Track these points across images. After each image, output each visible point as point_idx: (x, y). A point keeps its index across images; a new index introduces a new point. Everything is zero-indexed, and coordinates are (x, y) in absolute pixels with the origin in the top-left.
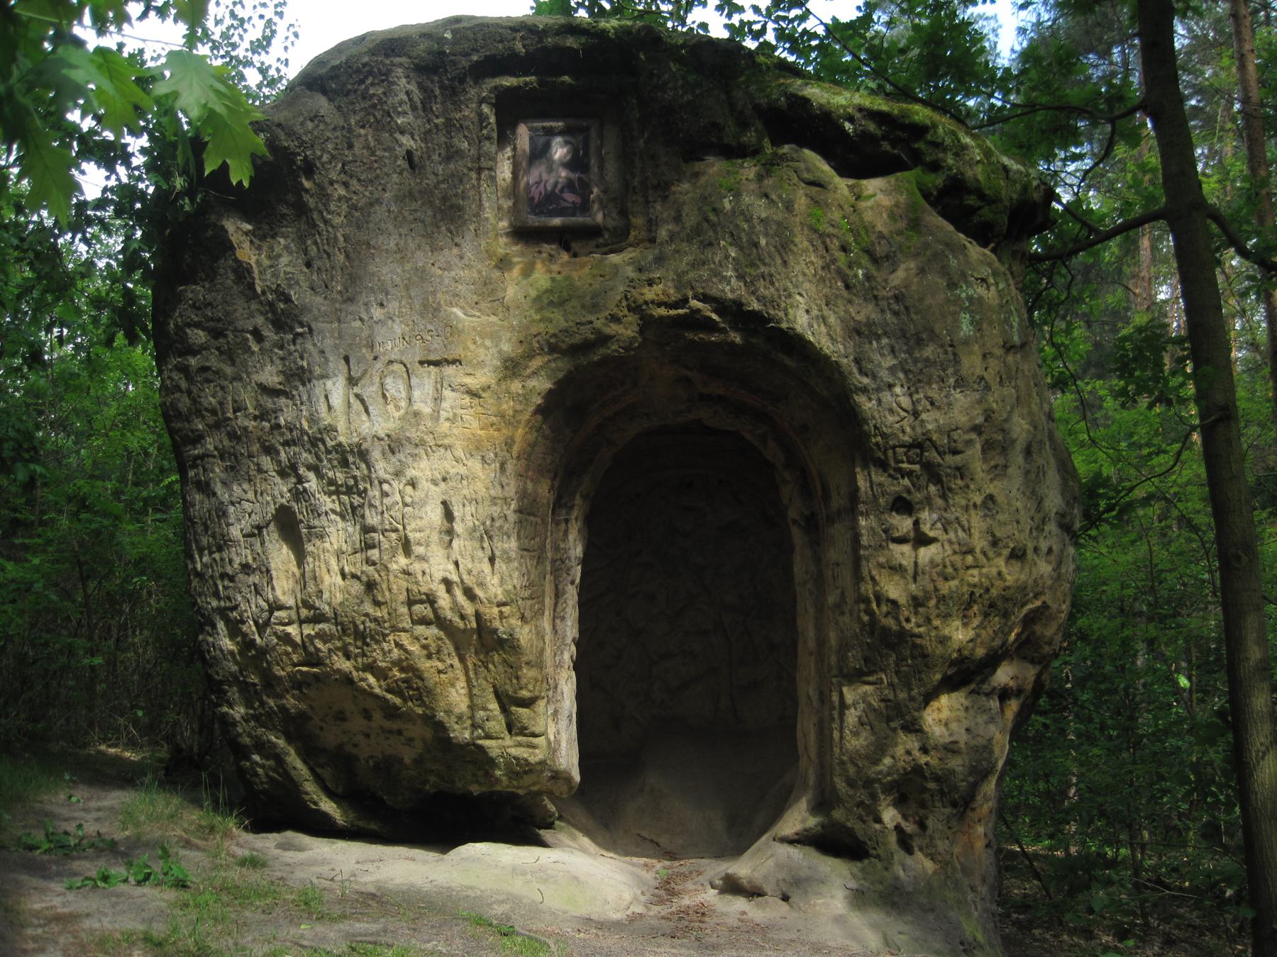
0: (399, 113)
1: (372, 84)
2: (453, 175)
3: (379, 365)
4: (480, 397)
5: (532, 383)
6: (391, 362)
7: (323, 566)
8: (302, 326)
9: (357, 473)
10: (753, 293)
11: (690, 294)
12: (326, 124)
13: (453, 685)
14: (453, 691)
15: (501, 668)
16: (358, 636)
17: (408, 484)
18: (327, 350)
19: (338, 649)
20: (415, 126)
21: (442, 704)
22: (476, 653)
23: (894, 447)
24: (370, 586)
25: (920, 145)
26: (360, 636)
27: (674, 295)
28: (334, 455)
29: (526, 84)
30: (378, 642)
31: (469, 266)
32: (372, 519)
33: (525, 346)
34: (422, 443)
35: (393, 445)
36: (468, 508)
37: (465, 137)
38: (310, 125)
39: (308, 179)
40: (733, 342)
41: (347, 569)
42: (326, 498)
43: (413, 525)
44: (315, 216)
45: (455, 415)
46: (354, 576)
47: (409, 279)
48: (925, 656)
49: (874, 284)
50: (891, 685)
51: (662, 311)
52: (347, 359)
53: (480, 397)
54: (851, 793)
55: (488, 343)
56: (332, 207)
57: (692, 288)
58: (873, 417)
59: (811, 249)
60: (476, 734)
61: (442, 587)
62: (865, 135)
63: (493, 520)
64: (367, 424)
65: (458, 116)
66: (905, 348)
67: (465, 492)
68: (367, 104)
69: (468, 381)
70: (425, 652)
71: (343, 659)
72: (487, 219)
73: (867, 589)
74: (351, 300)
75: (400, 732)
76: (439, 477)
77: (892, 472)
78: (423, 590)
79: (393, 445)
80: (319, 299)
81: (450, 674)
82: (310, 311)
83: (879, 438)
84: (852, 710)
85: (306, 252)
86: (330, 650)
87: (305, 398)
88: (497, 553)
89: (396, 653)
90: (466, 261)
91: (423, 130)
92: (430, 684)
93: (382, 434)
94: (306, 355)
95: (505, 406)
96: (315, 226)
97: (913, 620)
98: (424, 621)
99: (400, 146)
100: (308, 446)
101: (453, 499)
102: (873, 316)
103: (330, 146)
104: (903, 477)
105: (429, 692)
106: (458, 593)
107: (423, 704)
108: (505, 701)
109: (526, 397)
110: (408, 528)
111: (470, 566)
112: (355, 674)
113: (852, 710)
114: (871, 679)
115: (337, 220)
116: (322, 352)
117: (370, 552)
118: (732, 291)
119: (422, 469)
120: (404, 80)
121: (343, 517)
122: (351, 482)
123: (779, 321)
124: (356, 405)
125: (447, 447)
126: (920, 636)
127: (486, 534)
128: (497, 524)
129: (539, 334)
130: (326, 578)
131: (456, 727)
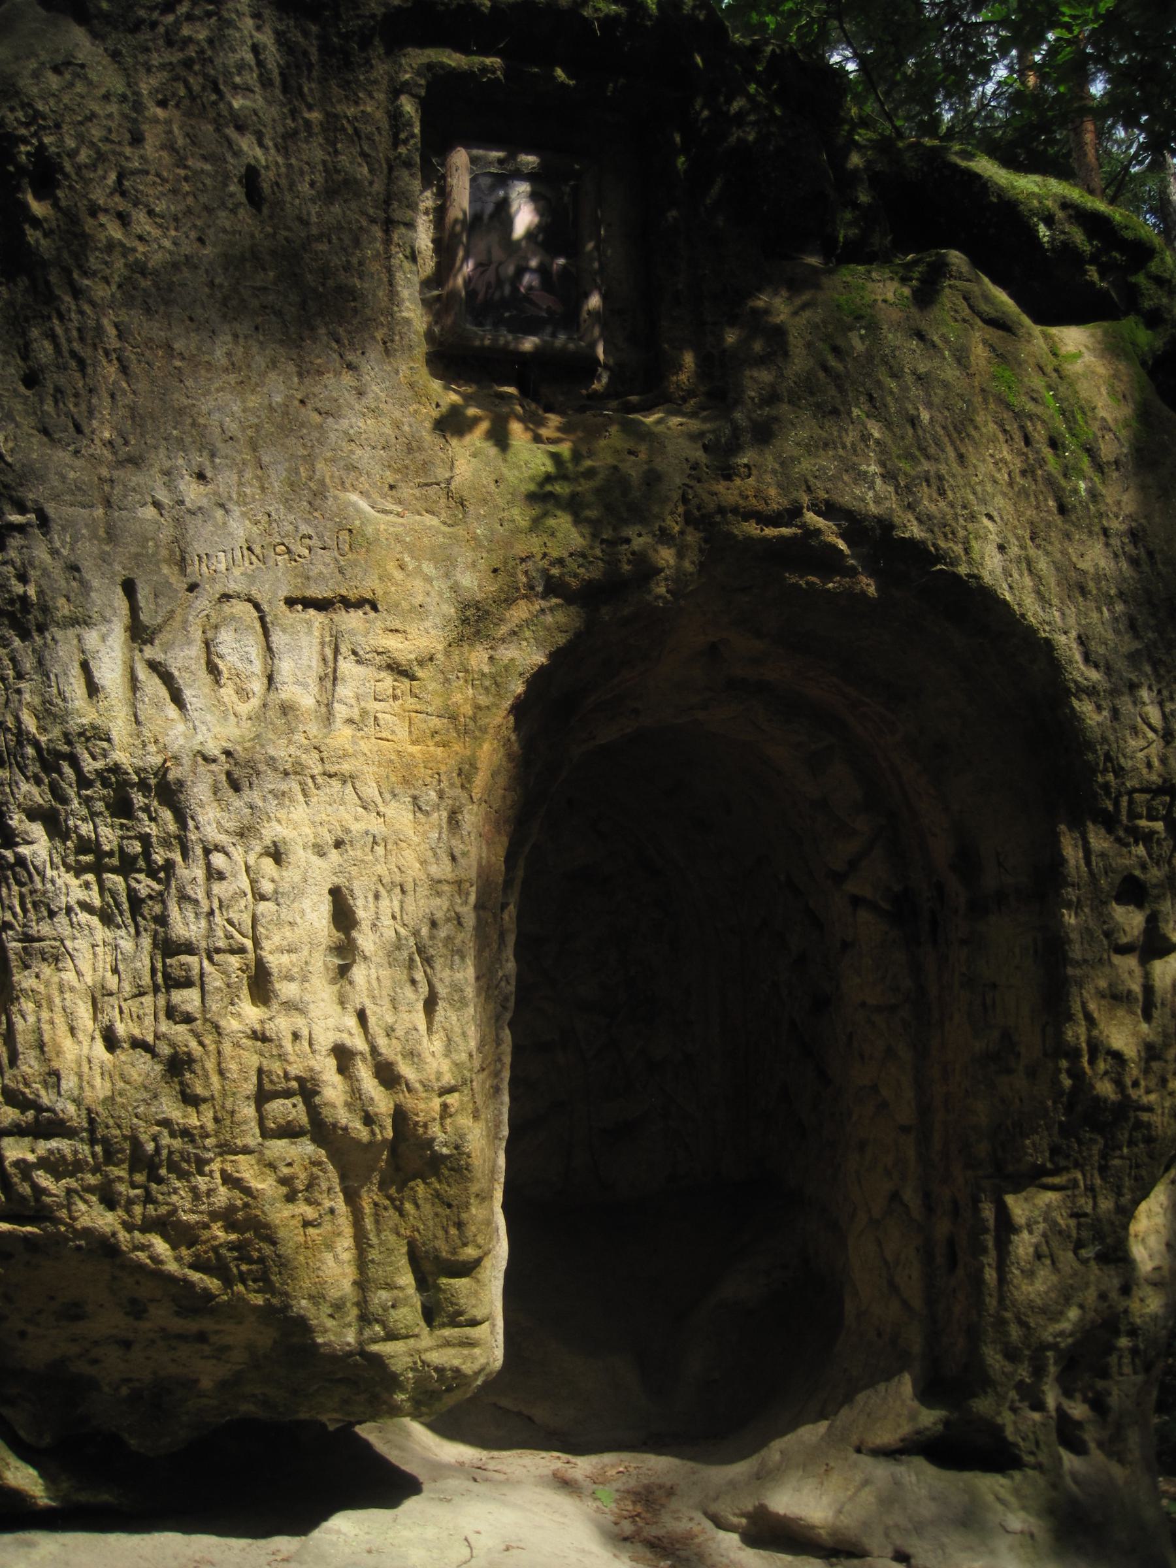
0: (236, 87)
1: (189, 17)
2: (340, 228)
3: (203, 602)
4: (413, 678)
5: (508, 653)
6: (226, 597)
7: (59, 1020)
8: (23, 510)
9: (152, 829)
10: (910, 507)
11: (805, 499)
12: (90, 83)
13: (330, 1247)
14: (328, 1257)
15: (427, 1209)
16: (136, 1161)
17: (267, 853)
18: (86, 565)
19: (90, 1189)
20: (267, 118)
21: (307, 1284)
22: (382, 1186)
23: (1131, 793)
24: (178, 1065)
25: (1140, 279)
26: (144, 1163)
27: (776, 500)
28: (98, 791)
29: (484, 70)
30: (183, 1175)
31: (375, 412)
32: (185, 925)
33: (502, 578)
34: (298, 769)
35: (237, 773)
36: (384, 903)
37: (364, 155)
38: (54, 81)
39: (38, 197)
40: (863, 593)
41: (121, 1029)
42: (69, 878)
43: (277, 939)
44: (54, 277)
45: (364, 713)
46: (137, 1044)
47: (258, 428)
48: (1149, 1140)
49: (1103, 508)
50: (1091, 1190)
51: (752, 529)
52: (129, 588)
53: (413, 678)
54: (1009, 1368)
55: (428, 568)
56: (93, 262)
57: (809, 490)
58: (1105, 740)
59: (1001, 437)
60: (367, 1333)
61: (332, 1063)
62: (1066, 250)
63: (434, 924)
64: (181, 727)
65: (351, 111)
66: (1152, 622)
67: (381, 869)
68: (175, 57)
69: (392, 643)
70: (284, 1190)
71: (99, 1208)
72: (408, 321)
73: (1076, 1033)
74: (135, 462)
75: (202, 1337)
76: (329, 839)
77: (1121, 833)
78: (293, 1071)
79: (238, 774)
80: (62, 456)
81: (327, 1227)
82: (42, 479)
83: (1111, 777)
84: (1025, 1235)
85: (25, 352)
86: (69, 1191)
87: (28, 664)
88: (442, 991)
89: (223, 1196)
90: (369, 400)
91: (280, 129)
92: (286, 1250)
93: (213, 750)
94: (33, 574)
95: (458, 698)
96: (50, 298)
97: (1143, 1083)
98: (289, 1132)
99: (237, 153)
100: (34, 768)
101: (357, 886)
102: (1102, 563)
103: (96, 133)
104: (1136, 843)
105: (283, 1263)
106: (364, 1073)
107: (267, 1286)
108: (427, 1266)
109: (497, 683)
110: (266, 944)
111: (390, 1019)
112: (123, 1235)
113: (1025, 1235)
114: (1056, 1180)
115: (101, 292)
116: (75, 568)
117: (177, 996)
118: (878, 501)
119: (295, 822)
120: (249, 22)
121: (107, 919)
122: (136, 847)
123: (954, 562)
124: (152, 685)
125: (345, 779)
126: (1149, 1109)
127: (417, 956)
128: (442, 933)
129: (530, 557)
130: (67, 1043)
131: (330, 1323)
